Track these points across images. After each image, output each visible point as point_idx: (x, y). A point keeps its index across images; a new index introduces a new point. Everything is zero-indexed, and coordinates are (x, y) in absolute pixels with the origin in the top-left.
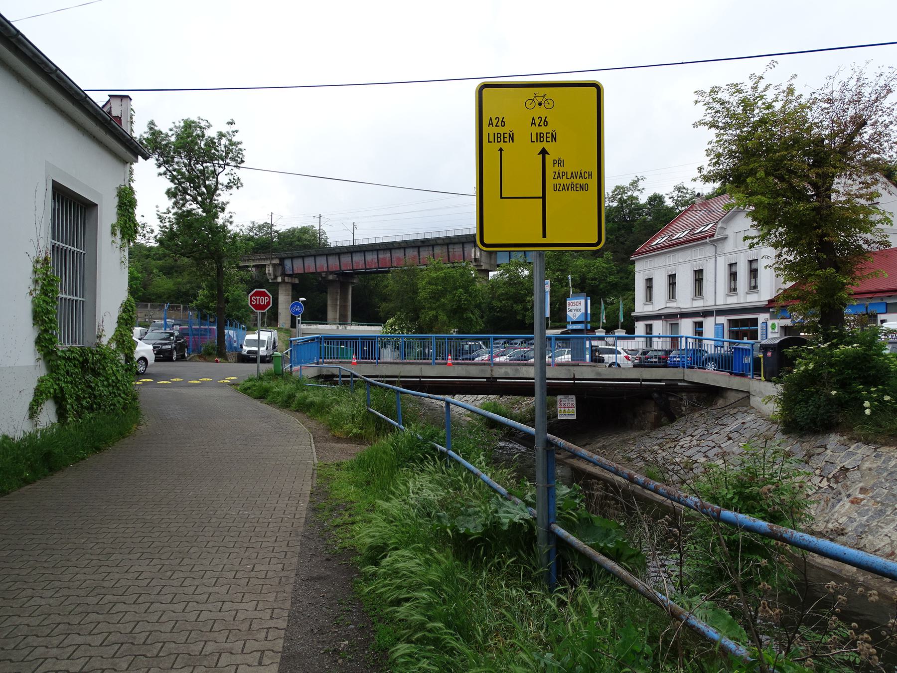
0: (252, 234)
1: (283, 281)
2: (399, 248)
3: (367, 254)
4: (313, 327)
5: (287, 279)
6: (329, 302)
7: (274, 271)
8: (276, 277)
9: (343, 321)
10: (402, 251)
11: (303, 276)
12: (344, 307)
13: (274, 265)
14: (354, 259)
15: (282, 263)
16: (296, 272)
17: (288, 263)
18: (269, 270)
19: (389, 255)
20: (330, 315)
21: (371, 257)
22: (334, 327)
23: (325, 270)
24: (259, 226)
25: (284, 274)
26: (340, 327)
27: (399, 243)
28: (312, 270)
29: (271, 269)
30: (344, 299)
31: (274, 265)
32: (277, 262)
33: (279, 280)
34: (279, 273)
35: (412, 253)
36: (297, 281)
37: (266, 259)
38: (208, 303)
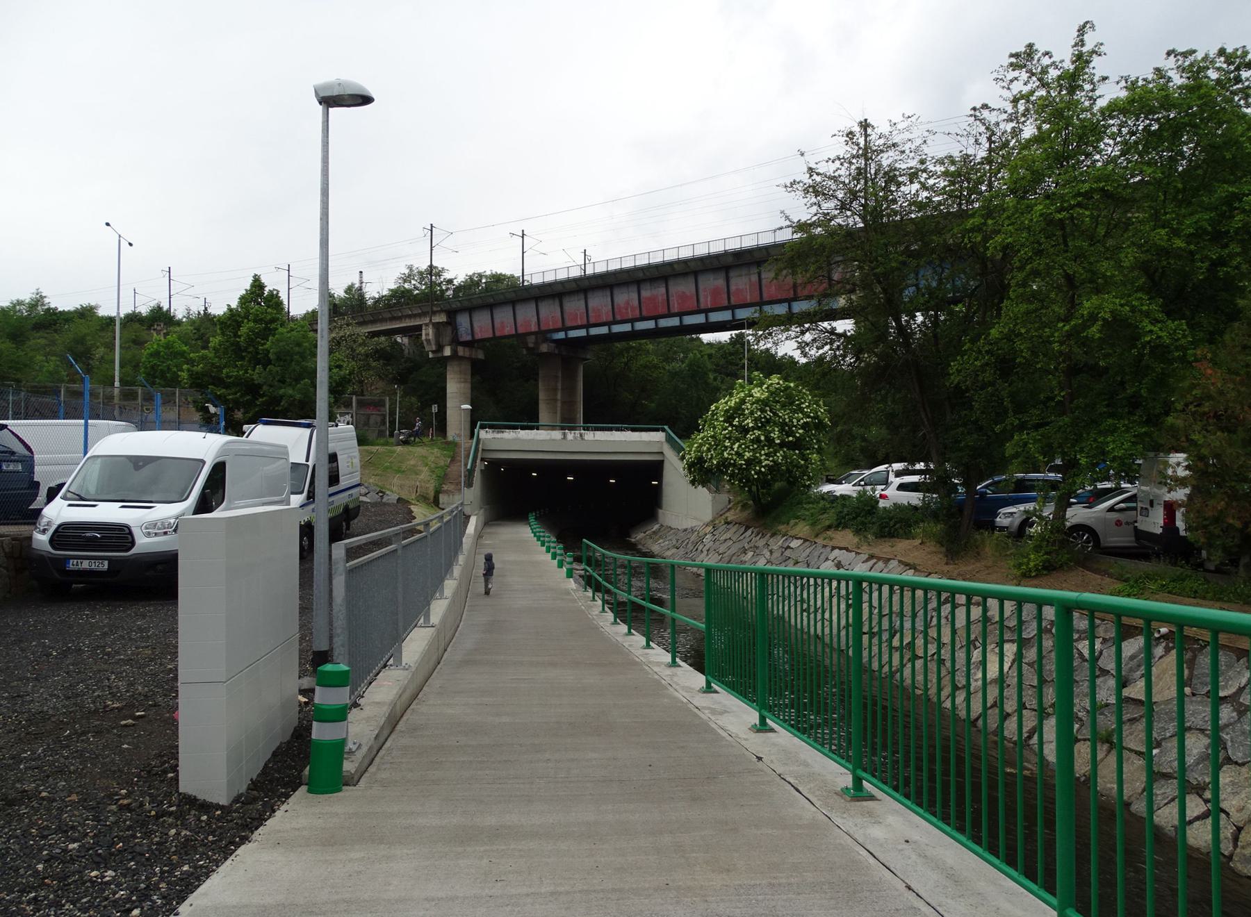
0: (407, 286)
1: (454, 352)
2: (684, 274)
3: (616, 292)
4: (509, 435)
6: (542, 396)
7: (438, 335)
8: (440, 348)
9: (567, 423)
10: (691, 280)
11: (495, 345)
12: (569, 405)
13: (437, 326)
14: (733, 282)
15: (451, 323)
16: (478, 336)
17: (463, 320)
18: (428, 333)
19: (662, 290)
20: (544, 416)
21: (626, 298)
22: (557, 435)
23: (534, 328)
24: (421, 273)
25: (456, 342)
26: (570, 435)
27: (685, 262)
28: (509, 330)
29: (431, 331)
30: (570, 389)
31: (437, 326)
32: (441, 318)
33: (447, 352)
34: (447, 337)
35: (712, 282)
37: (423, 314)
38: (220, 369)
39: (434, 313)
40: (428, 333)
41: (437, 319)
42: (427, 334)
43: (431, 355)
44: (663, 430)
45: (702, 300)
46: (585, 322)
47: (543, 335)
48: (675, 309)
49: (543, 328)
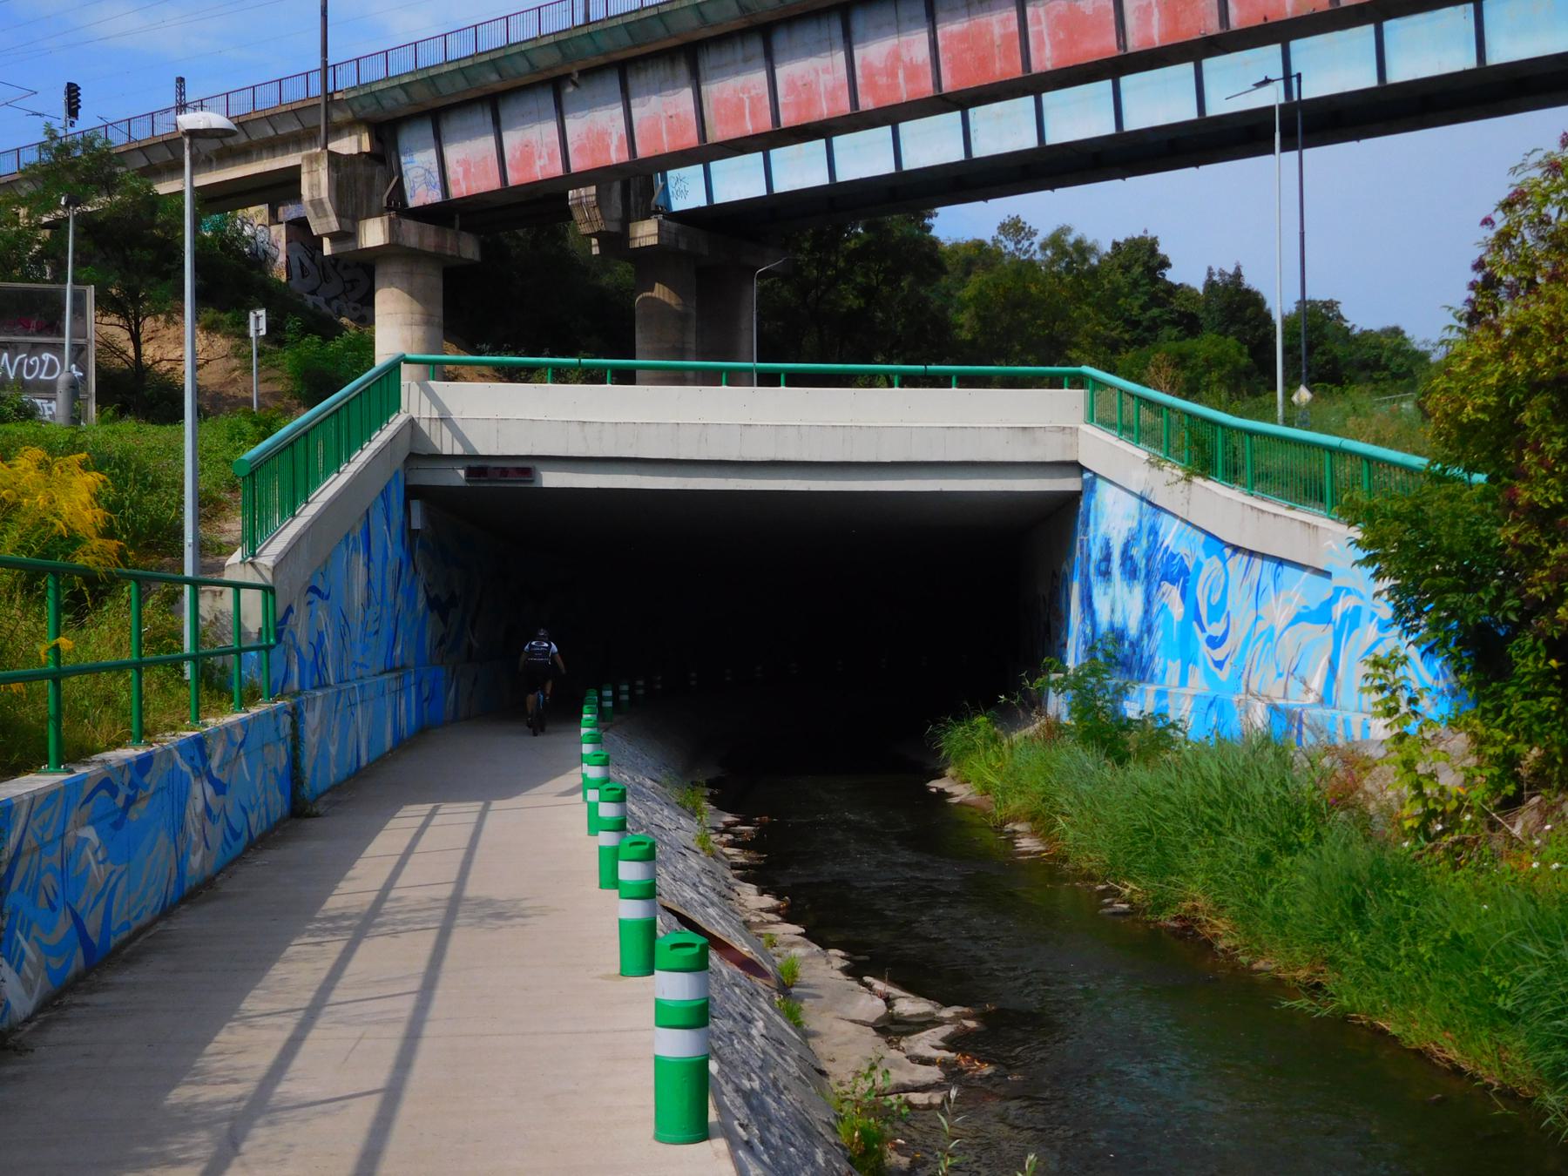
5: (413, 234)
15: (384, 156)
16: (458, 190)
18: (316, 183)
28: (545, 166)
32: (349, 145)
36: (470, 250)
39: (336, 131)
40: (316, 183)
41: (347, 145)
42: (314, 186)
43: (327, 249)
44: (1078, 382)
45: (1131, 21)
46: (766, 125)
47: (636, 182)
48: (1045, 59)
49: (642, 152)
